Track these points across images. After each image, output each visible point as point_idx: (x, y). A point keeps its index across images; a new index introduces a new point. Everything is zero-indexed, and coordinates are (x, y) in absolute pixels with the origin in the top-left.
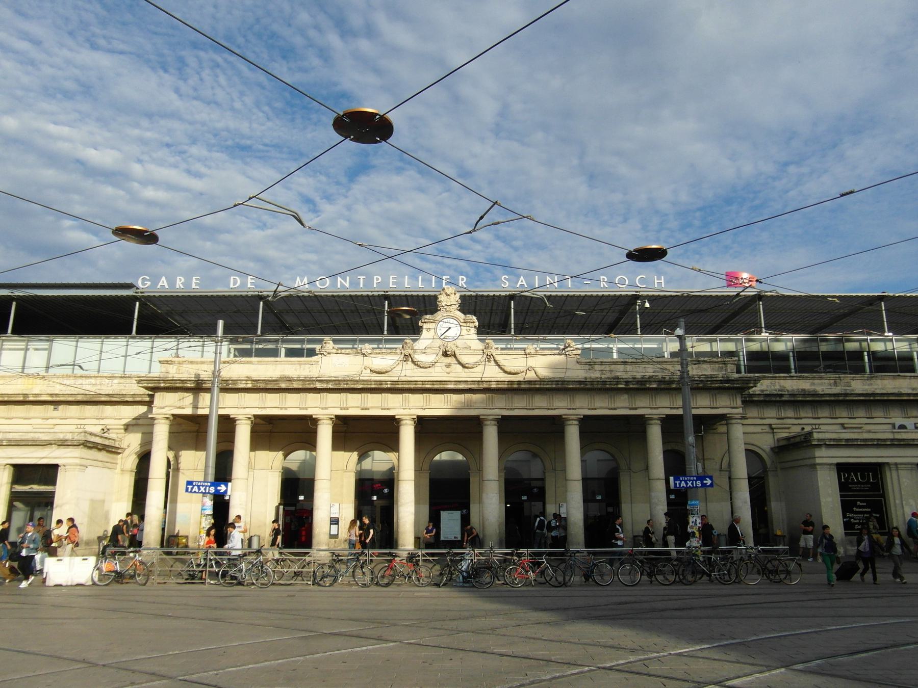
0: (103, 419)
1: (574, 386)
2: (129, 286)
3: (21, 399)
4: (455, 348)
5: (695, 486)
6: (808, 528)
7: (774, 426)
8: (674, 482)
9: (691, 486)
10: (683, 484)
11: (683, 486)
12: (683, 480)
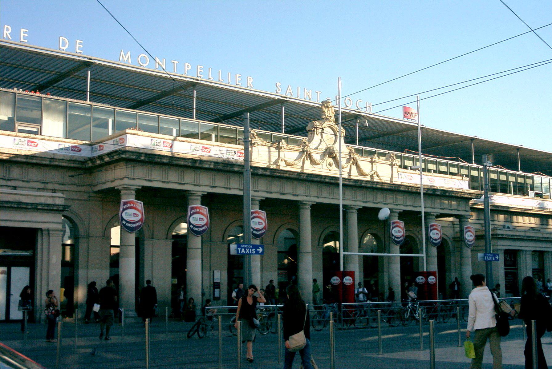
3: (48, 163)
5: (251, 253)
8: (237, 248)
9: (249, 253)
10: (243, 251)
11: (243, 253)
12: (243, 248)
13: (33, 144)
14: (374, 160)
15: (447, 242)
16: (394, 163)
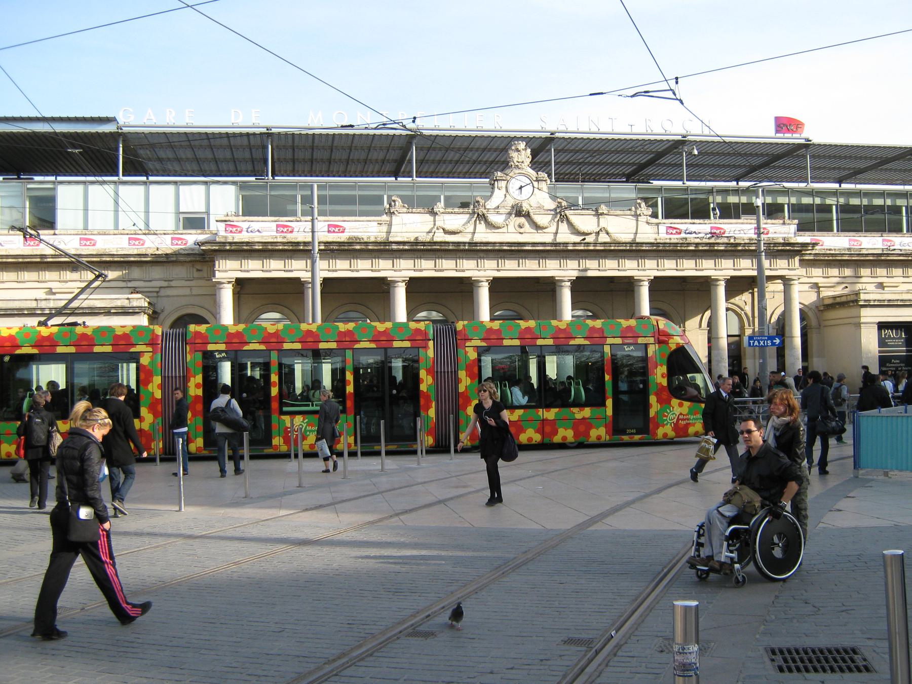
0: (130, 281)
1: (647, 248)
2: (108, 120)
4: (528, 207)
6: (471, 417)
7: (820, 285)
13: (88, 243)
14: (600, 211)
15: (806, 313)
16: (638, 212)
